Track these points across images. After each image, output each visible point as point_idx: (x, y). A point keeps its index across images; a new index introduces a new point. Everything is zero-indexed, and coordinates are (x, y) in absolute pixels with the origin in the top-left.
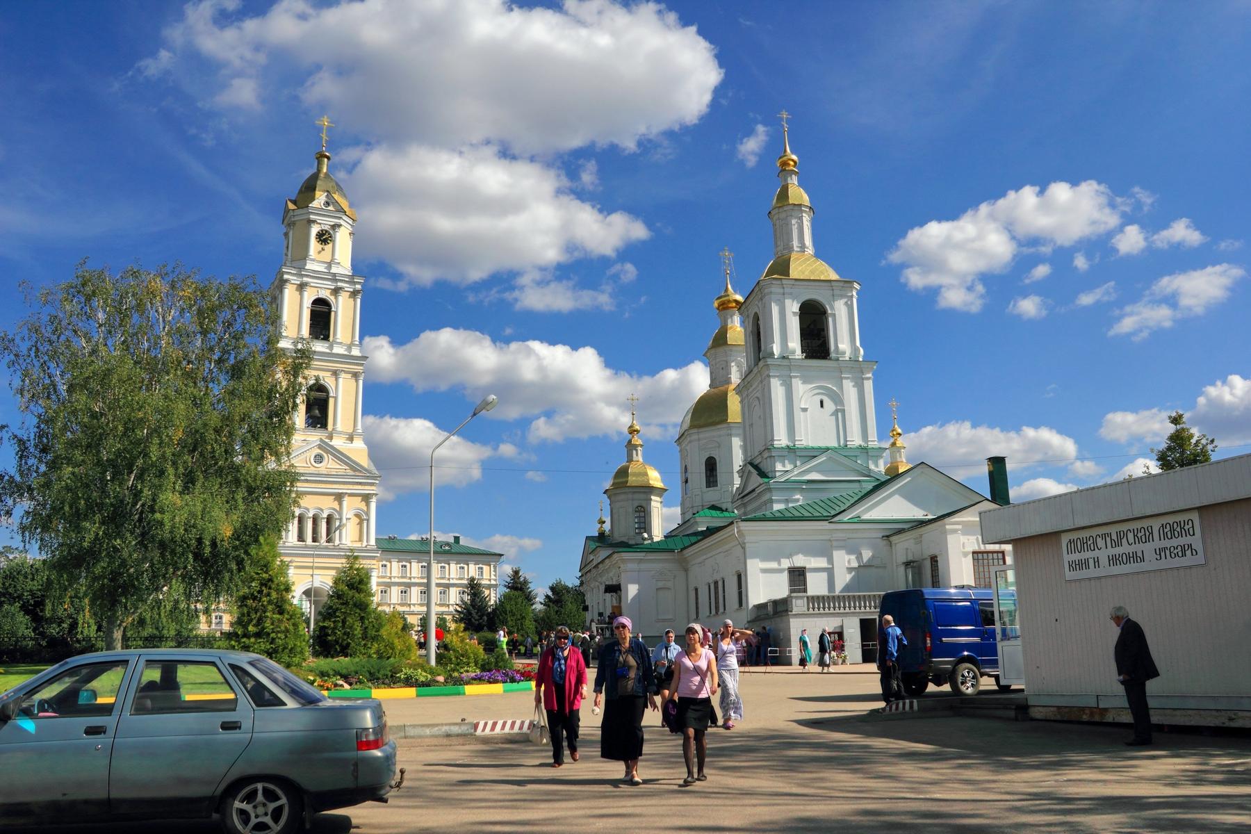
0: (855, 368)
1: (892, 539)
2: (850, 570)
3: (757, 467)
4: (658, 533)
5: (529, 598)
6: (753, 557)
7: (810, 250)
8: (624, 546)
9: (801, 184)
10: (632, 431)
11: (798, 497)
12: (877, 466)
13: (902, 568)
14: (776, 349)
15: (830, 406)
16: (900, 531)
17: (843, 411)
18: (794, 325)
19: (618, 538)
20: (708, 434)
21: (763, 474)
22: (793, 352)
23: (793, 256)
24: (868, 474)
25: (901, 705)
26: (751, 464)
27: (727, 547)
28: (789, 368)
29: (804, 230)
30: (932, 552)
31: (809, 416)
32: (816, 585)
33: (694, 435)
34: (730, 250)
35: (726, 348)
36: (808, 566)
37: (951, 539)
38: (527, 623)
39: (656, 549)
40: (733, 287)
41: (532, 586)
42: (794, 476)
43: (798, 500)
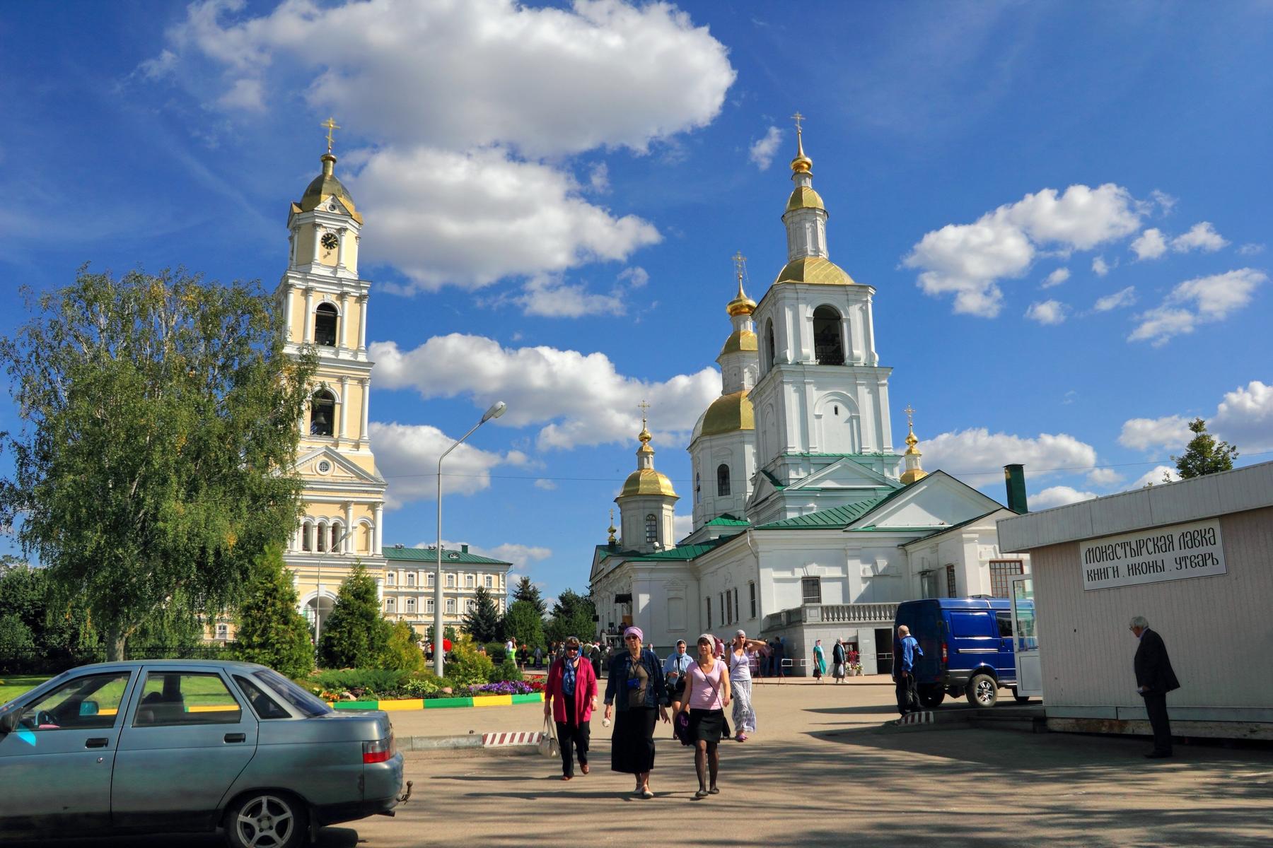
0: (870, 375)
1: (907, 548)
2: (865, 579)
3: (771, 475)
4: (669, 542)
5: (538, 608)
6: (767, 566)
7: (824, 254)
8: (635, 555)
9: (815, 187)
10: (643, 438)
11: (812, 505)
12: (892, 474)
13: (918, 578)
14: (790, 355)
15: (844, 413)
16: (916, 540)
17: (858, 418)
18: (808, 331)
19: (629, 547)
20: (720, 441)
21: (776, 482)
22: (807, 358)
23: (807, 261)
24: (883, 482)
25: (917, 717)
26: (764, 472)
27: (740, 556)
28: (803, 374)
29: (818, 234)
30: (949, 561)
31: (824, 423)
32: (831, 595)
33: (706, 442)
34: (742, 255)
35: (738, 354)
36: (822, 576)
37: (968, 548)
38: (536, 633)
39: (667, 558)
40: (746, 292)
41: (541, 596)
42: (808, 484)
43: (812, 509)
